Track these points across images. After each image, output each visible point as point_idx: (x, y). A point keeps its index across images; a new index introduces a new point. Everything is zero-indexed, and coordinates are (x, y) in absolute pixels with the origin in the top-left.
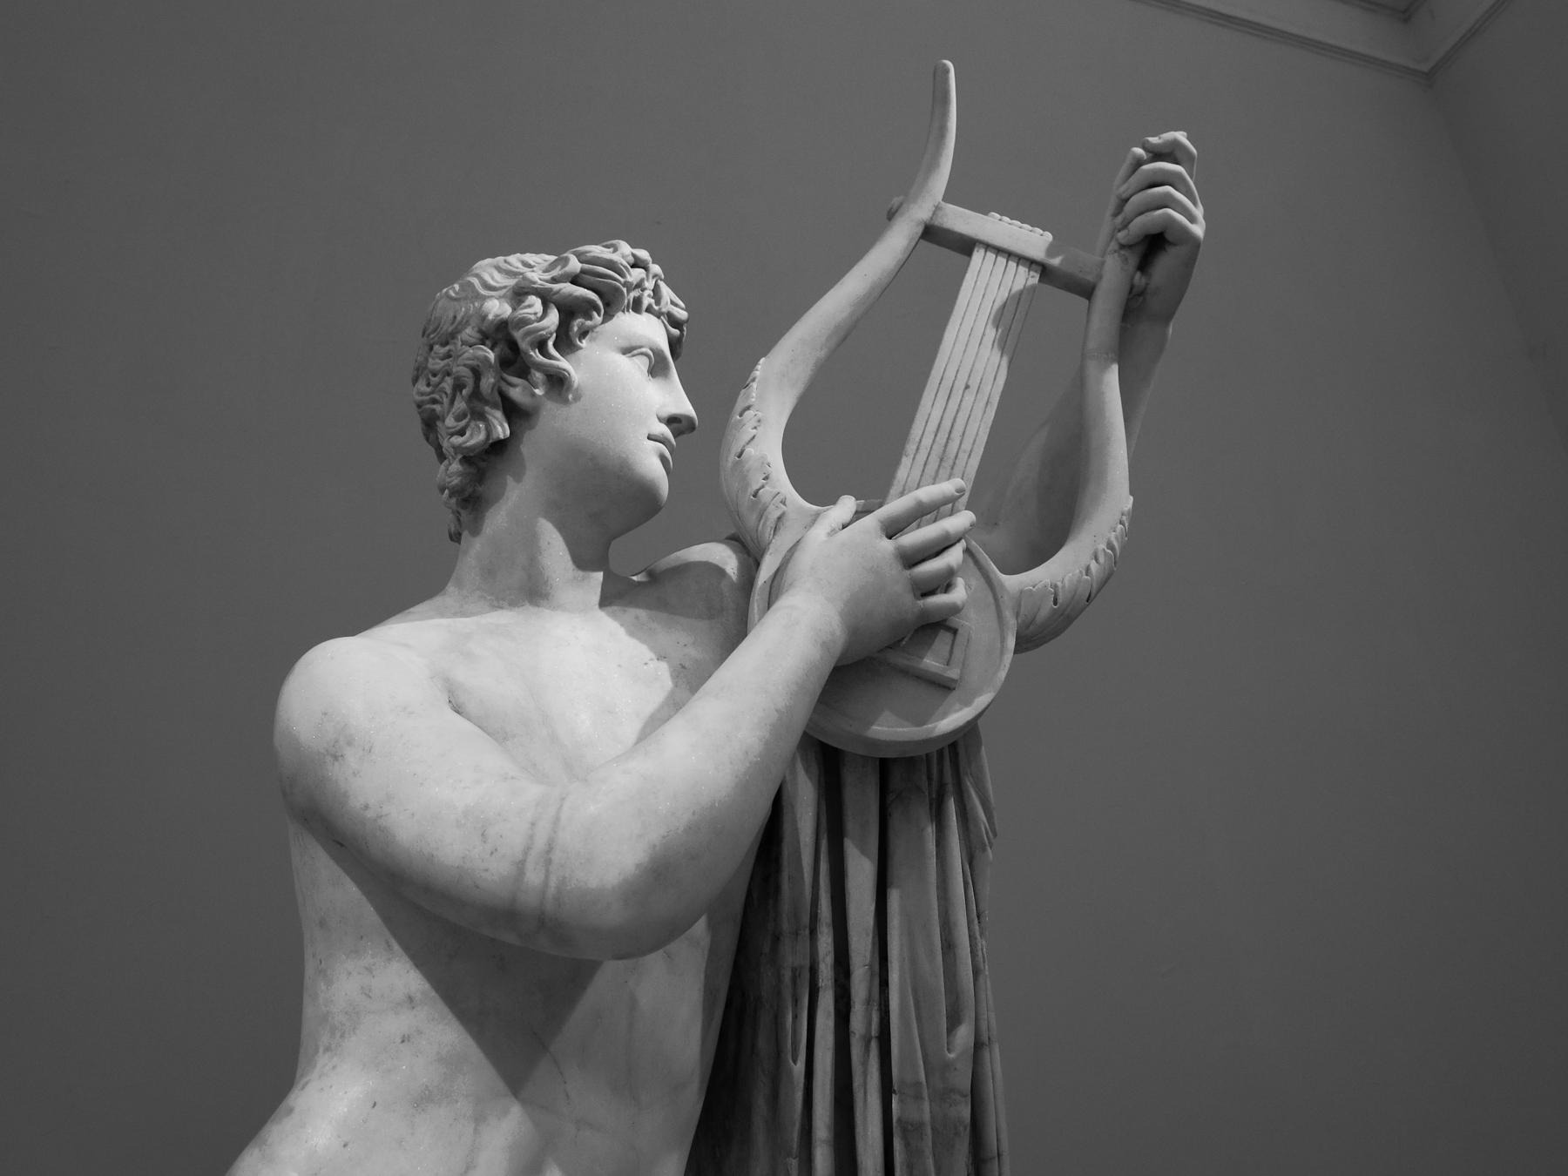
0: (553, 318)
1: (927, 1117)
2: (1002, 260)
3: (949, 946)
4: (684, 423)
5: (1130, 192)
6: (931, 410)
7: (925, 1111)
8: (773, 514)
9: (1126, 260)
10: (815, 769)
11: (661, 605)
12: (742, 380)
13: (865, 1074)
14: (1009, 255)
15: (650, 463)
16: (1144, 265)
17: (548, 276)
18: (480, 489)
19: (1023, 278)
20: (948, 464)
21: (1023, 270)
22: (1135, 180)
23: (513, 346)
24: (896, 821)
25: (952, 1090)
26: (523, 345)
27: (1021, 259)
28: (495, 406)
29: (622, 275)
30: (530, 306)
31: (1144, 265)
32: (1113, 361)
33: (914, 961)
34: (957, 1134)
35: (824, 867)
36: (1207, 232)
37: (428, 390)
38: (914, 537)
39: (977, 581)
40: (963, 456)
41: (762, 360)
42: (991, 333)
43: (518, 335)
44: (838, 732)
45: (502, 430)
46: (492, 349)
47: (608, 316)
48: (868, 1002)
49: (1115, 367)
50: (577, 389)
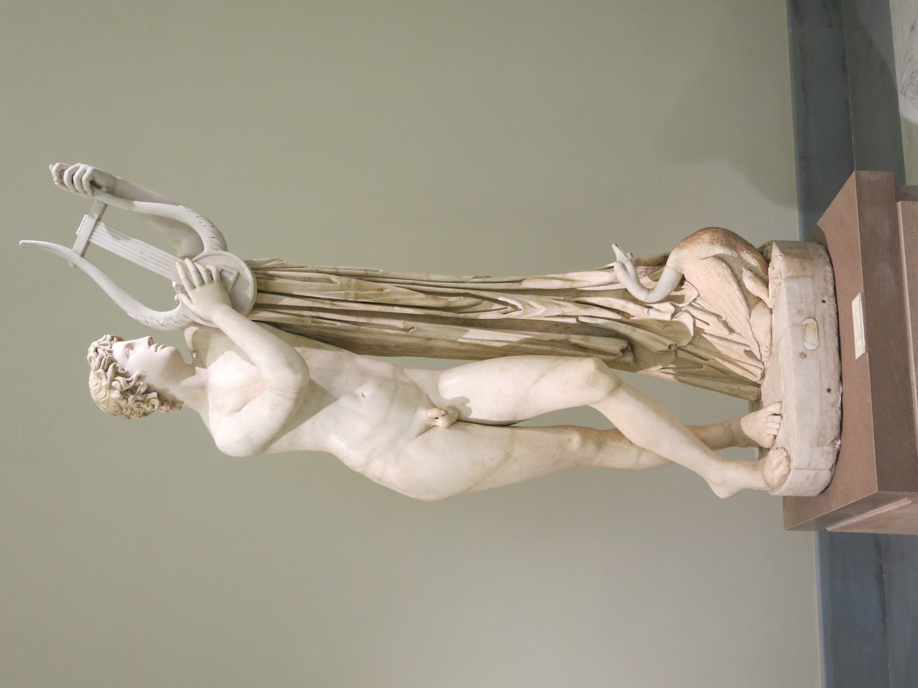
0: (119, 378)
1: (353, 292)
2: (95, 233)
4: (151, 340)
6: (149, 265)
7: (352, 292)
9: (97, 194)
10: (257, 311)
13: (341, 306)
15: (165, 352)
16: (99, 187)
17: (104, 379)
18: (170, 401)
19: (102, 227)
21: (98, 227)
22: (70, 187)
23: (127, 390)
25: (348, 284)
26: (128, 387)
28: (147, 396)
29: (103, 357)
30: (116, 385)
31: (99, 187)
32: (133, 203)
34: (359, 284)
35: (285, 311)
36: (91, 165)
38: (196, 281)
41: (129, 314)
42: (123, 242)
43: (125, 389)
44: (249, 305)
45: (155, 395)
46: (129, 396)
47: (116, 361)
48: (323, 303)
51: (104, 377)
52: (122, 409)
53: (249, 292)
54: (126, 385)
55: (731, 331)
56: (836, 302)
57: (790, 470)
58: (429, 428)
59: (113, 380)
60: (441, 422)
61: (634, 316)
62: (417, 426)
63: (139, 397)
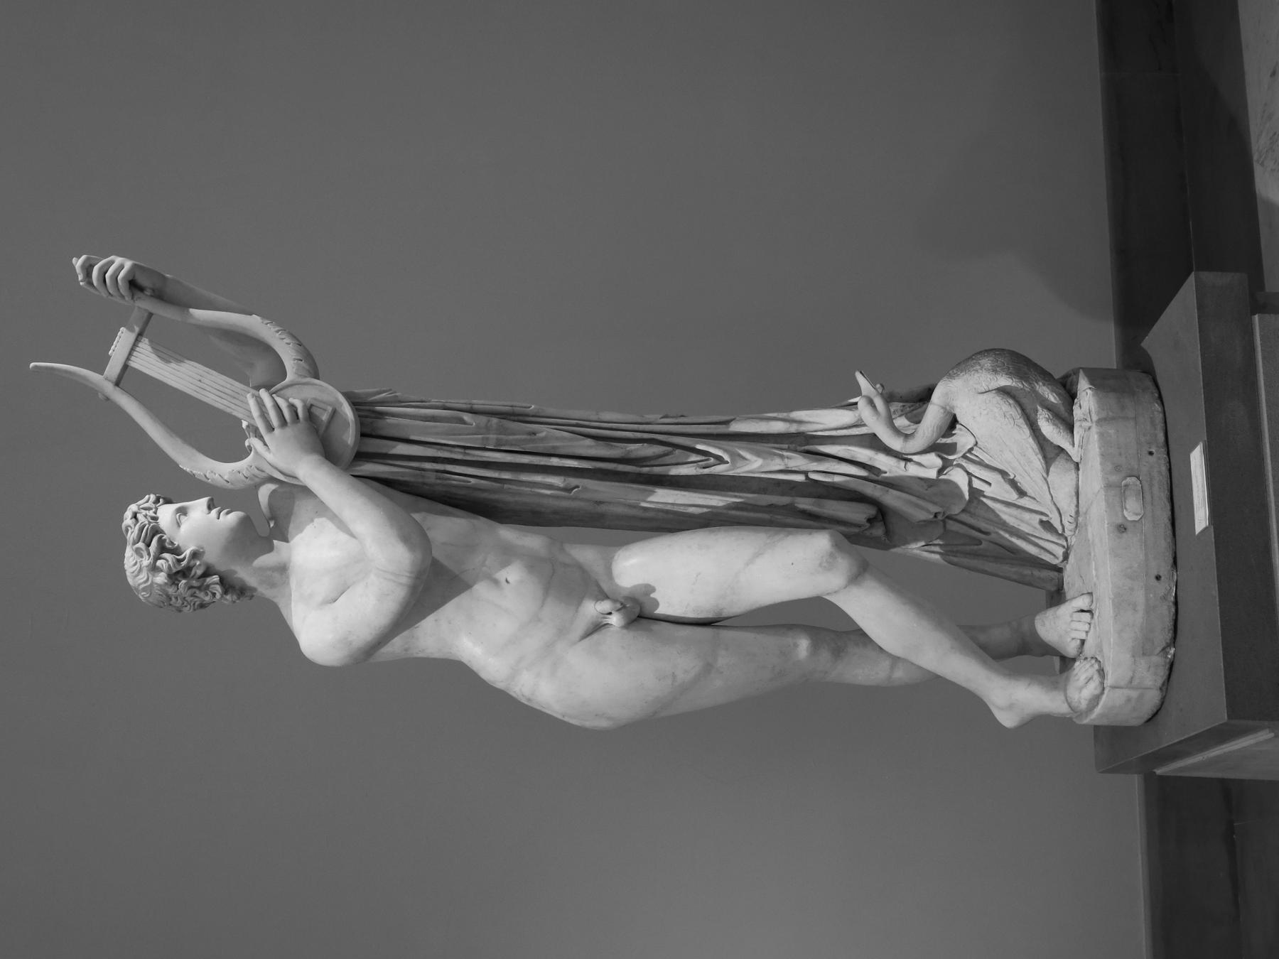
0: (166, 555)
1: (495, 436)
2: (135, 353)
3: (433, 419)
5: (106, 292)
6: (211, 398)
7: (493, 437)
8: (257, 472)
9: (139, 298)
10: (361, 463)
11: (289, 516)
12: (191, 477)
14: (132, 350)
16: (141, 289)
18: (237, 587)
19: (145, 346)
20: (236, 395)
21: (140, 345)
23: (178, 572)
24: (384, 433)
25: (486, 425)
26: (179, 568)
27: (135, 345)
28: (205, 581)
29: (144, 526)
30: (163, 565)
33: (437, 434)
36: (130, 258)
37: (189, 606)
38: (275, 421)
39: (288, 392)
40: (233, 388)
42: (173, 365)
43: (174, 570)
44: (348, 455)
45: (216, 578)
46: (180, 581)
47: (162, 532)
48: (451, 452)
49: (192, 310)
50: (198, 547)
51: (145, 553)
52: (171, 599)
53: (349, 437)
54: (176, 565)
55: (1022, 493)
56: (1168, 454)
57: (1104, 689)
58: (598, 627)
59: (157, 558)
60: (615, 620)
61: (886, 473)
62: (581, 625)
63: (194, 582)
